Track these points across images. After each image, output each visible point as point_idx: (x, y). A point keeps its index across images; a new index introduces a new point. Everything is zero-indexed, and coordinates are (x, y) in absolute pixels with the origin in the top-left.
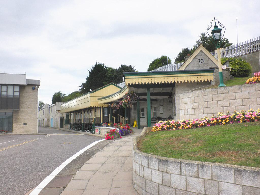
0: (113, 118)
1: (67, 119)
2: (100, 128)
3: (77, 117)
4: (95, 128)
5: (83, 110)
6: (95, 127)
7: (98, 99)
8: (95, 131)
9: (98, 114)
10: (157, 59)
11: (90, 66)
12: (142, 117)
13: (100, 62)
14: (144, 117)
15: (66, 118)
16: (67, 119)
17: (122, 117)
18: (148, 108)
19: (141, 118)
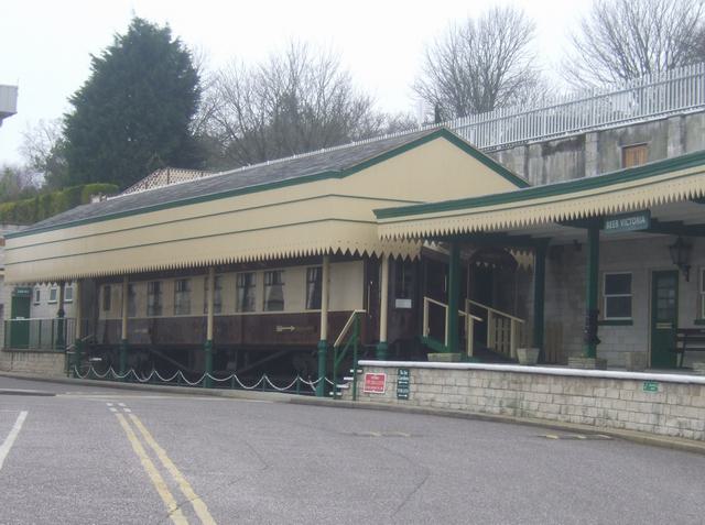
0: (462, 320)
1: (18, 319)
2: (408, 369)
3: (107, 308)
4: (361, 367)
5: (211, 270)
6: (361, 362)
7: (380, 213)
8: (362, 384)
9: (347, 297)
10: (161, 26)
11: (102, 38)
12: (606, 319)
13: (157, 20)
14: (630, 323)
15: (13, 316)
16: (18, 319)
17: (498, 316)
18: (41, 294)
19: (605, 327)
